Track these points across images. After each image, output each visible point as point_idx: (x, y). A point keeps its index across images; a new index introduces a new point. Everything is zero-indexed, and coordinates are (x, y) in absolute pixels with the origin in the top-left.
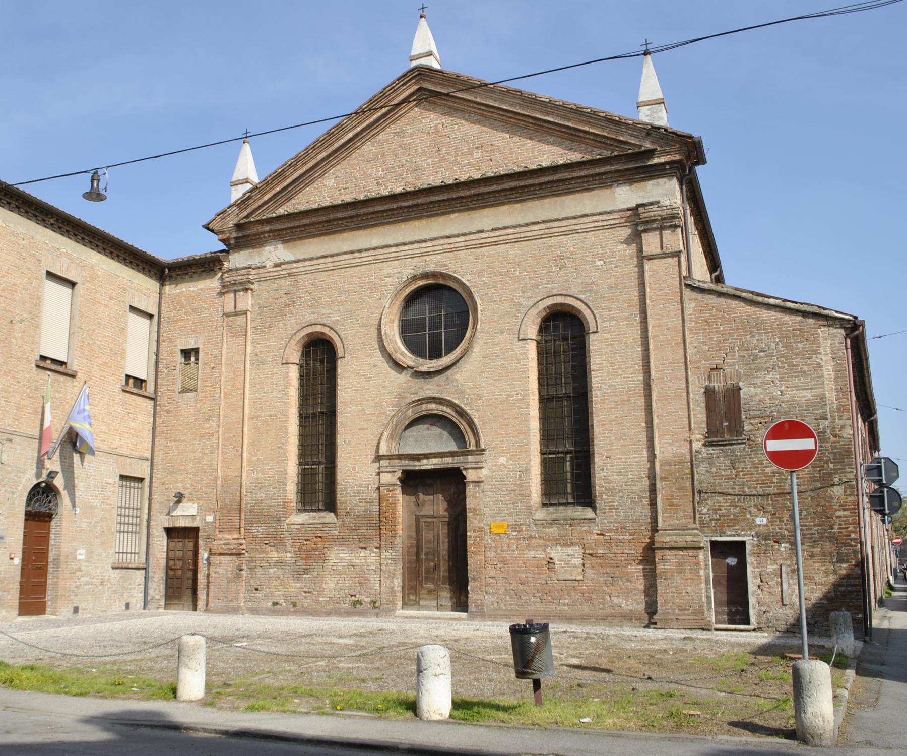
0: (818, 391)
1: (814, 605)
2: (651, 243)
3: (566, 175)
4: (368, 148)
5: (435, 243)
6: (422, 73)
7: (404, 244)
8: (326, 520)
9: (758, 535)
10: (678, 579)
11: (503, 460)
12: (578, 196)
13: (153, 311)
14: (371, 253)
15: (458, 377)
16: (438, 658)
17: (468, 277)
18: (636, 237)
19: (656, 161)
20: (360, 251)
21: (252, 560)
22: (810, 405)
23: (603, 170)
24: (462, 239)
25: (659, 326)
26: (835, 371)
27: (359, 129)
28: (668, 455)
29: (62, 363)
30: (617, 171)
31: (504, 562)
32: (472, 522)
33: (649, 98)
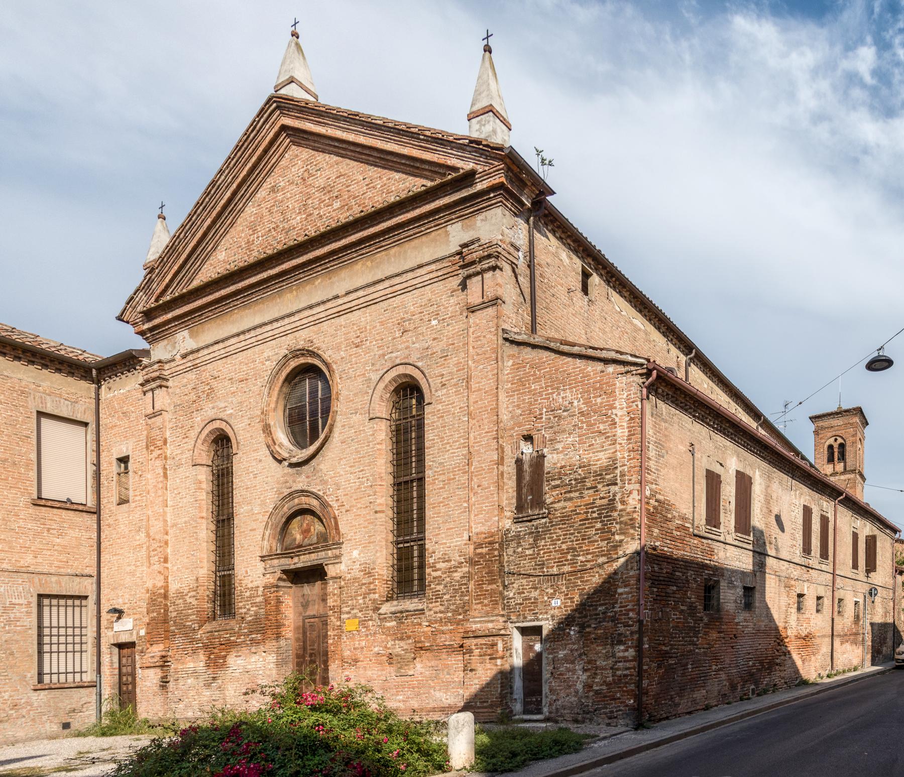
11: (355, 553)
13: (90, 418)
14: (253, 333)
15: (322, 466)
26: (628, 427)
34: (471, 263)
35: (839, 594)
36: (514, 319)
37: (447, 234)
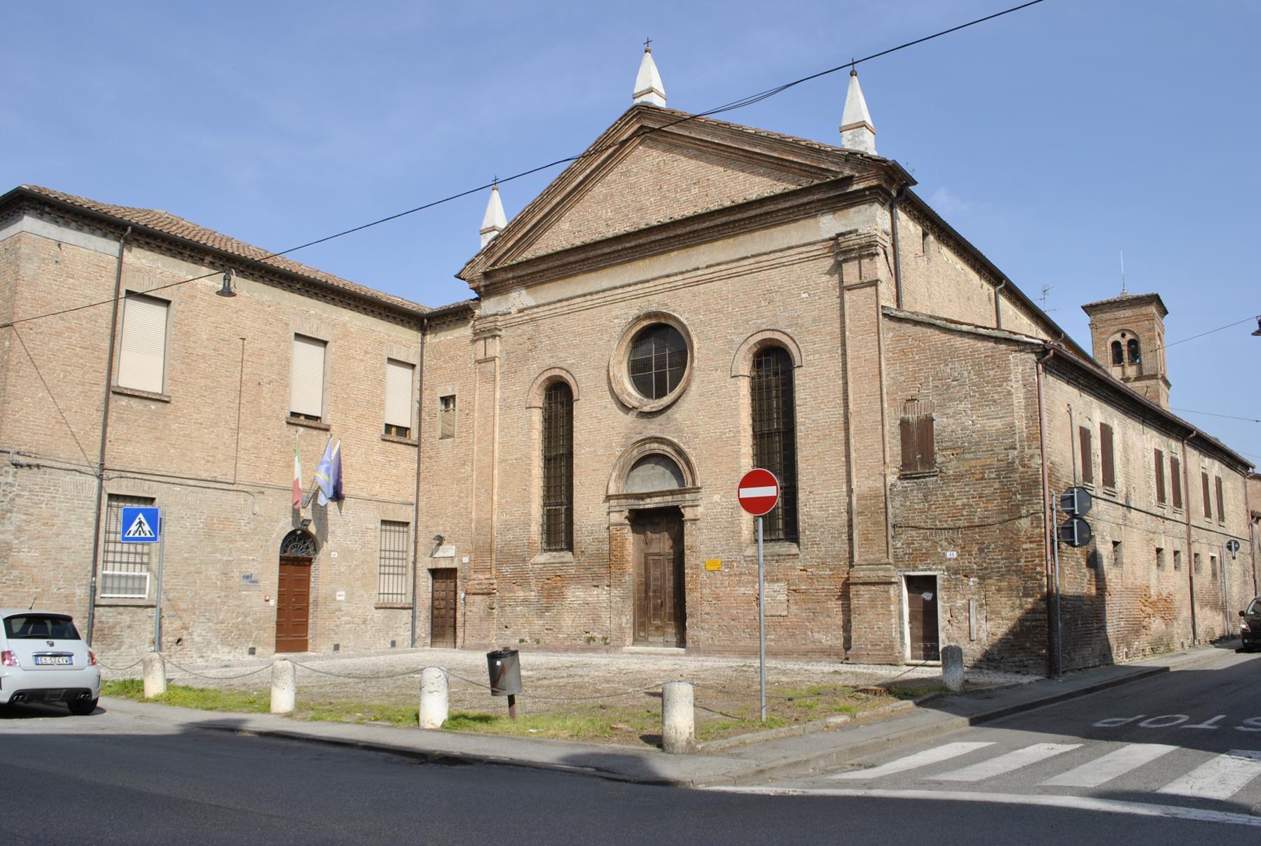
0: (1008, 420)
1: (1000, 640)
2: (851, 272)
3: (771, 208)
4: (599, 190)
5: (657, 282)
6: (643, 111)
7: (629, 285)
8: (564, 560)
9: (948, 569)
10: (870, 615)
11: (716, 498)
12: (785, 227)
14: (601, 295)
15: (677, 416)
16: (434, 679)
17: (687, 315)
18: (837, 269)
19: (855, 187)
20: (591, 294)
21: (502, 599)
22: (1000, 435)
23: (805, 200)
24: (680, 277)
25: (858, 358)
27: (588, 171)
28: (865, 489)
29: (317, 418)
30: (819, 200)
31: (718, 598)
32: (690, 559)
33: (857, 123)
34: (844, 251)
35: (1196, 548)
36: (887, 297)
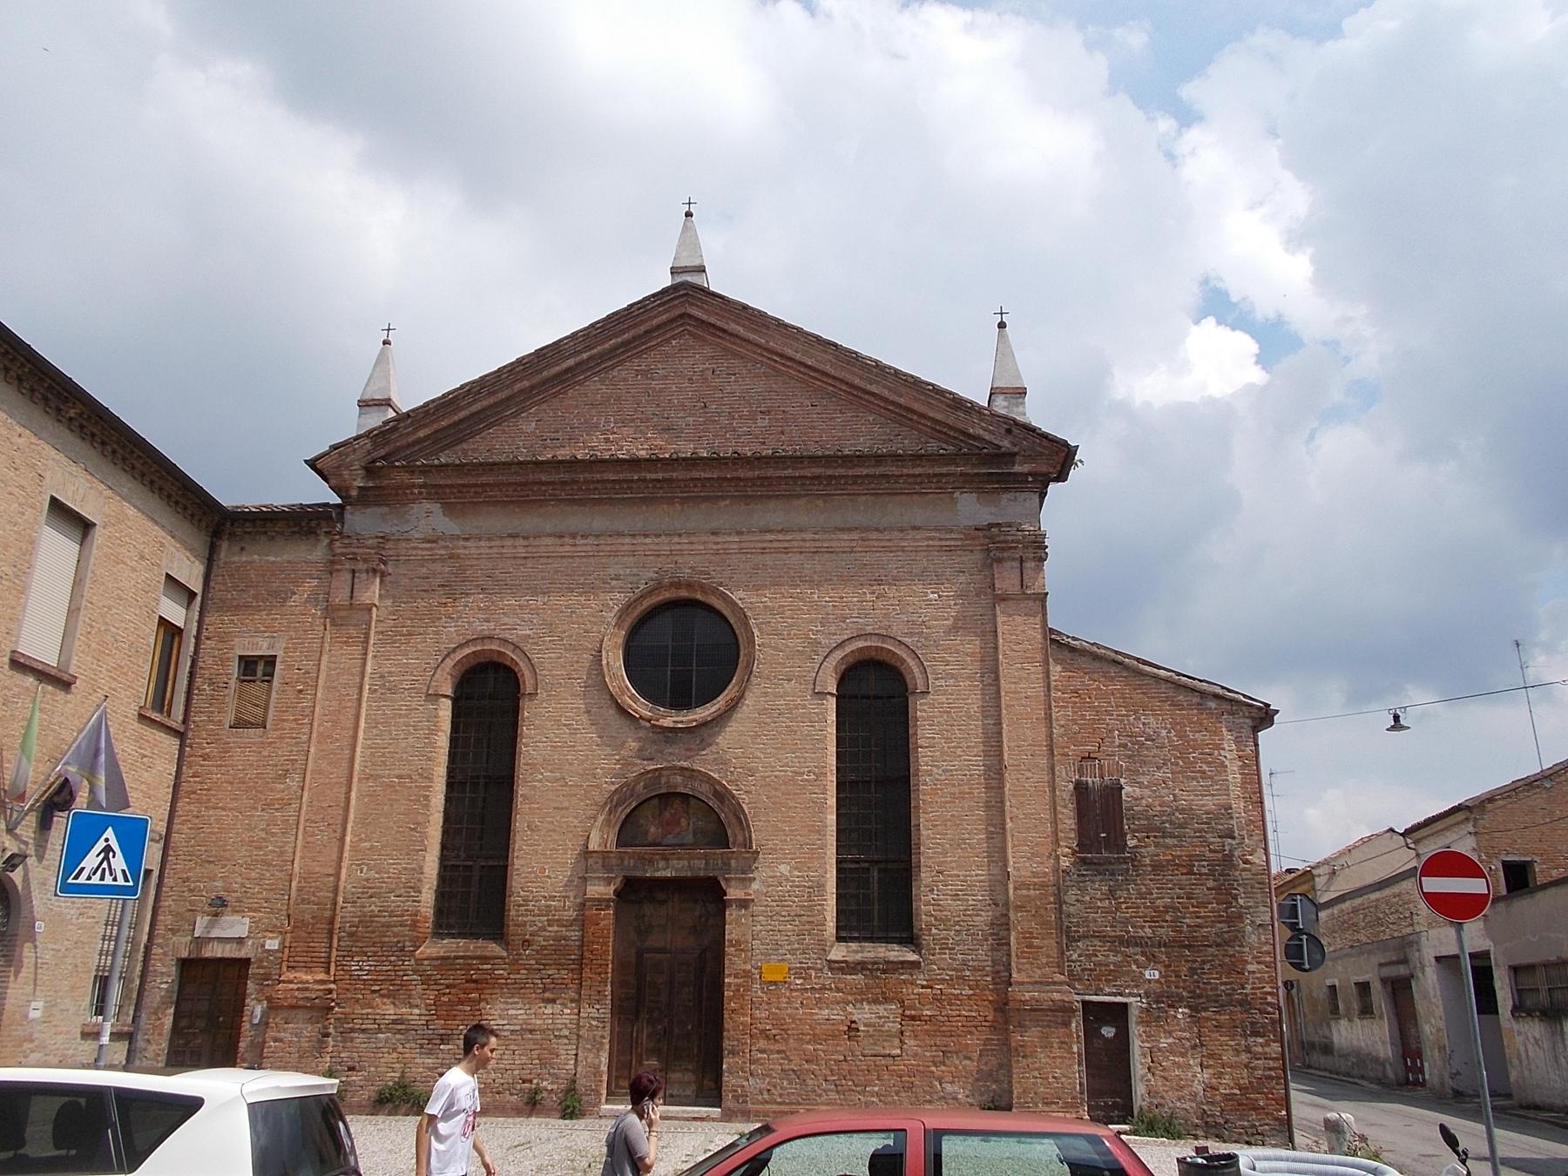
0: (1222, 799)
3: (892, 470)
9: (1147, 995)
10: (1042, 1057)
11: (784, 869)
15: (719, 739)
19: (1018, 469)
37: (954, 501)
